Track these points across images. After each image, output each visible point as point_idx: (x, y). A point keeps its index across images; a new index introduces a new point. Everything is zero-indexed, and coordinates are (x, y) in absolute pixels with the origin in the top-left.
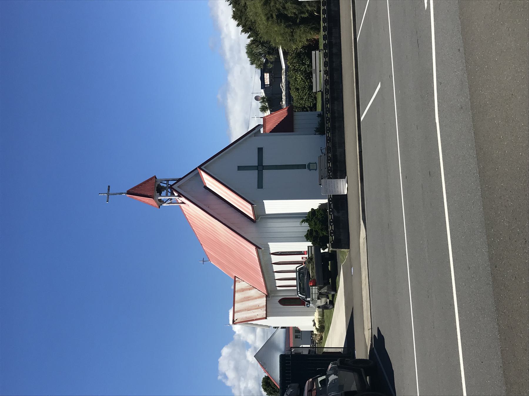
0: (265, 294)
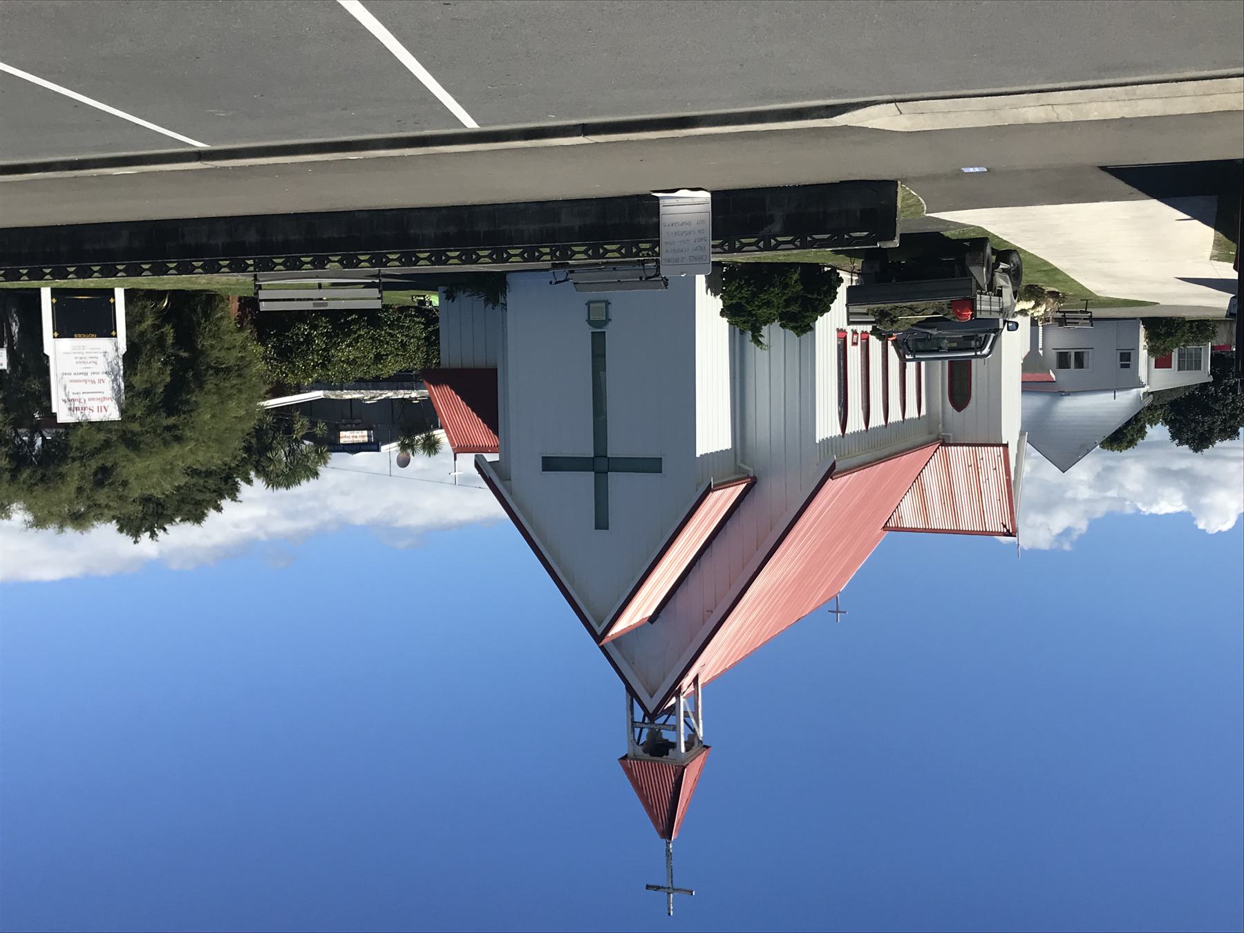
0: (938, 448)
